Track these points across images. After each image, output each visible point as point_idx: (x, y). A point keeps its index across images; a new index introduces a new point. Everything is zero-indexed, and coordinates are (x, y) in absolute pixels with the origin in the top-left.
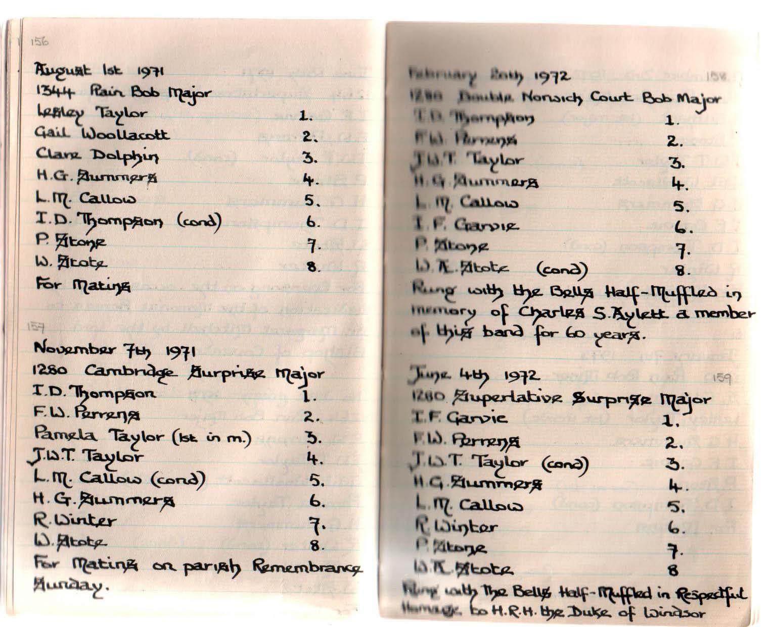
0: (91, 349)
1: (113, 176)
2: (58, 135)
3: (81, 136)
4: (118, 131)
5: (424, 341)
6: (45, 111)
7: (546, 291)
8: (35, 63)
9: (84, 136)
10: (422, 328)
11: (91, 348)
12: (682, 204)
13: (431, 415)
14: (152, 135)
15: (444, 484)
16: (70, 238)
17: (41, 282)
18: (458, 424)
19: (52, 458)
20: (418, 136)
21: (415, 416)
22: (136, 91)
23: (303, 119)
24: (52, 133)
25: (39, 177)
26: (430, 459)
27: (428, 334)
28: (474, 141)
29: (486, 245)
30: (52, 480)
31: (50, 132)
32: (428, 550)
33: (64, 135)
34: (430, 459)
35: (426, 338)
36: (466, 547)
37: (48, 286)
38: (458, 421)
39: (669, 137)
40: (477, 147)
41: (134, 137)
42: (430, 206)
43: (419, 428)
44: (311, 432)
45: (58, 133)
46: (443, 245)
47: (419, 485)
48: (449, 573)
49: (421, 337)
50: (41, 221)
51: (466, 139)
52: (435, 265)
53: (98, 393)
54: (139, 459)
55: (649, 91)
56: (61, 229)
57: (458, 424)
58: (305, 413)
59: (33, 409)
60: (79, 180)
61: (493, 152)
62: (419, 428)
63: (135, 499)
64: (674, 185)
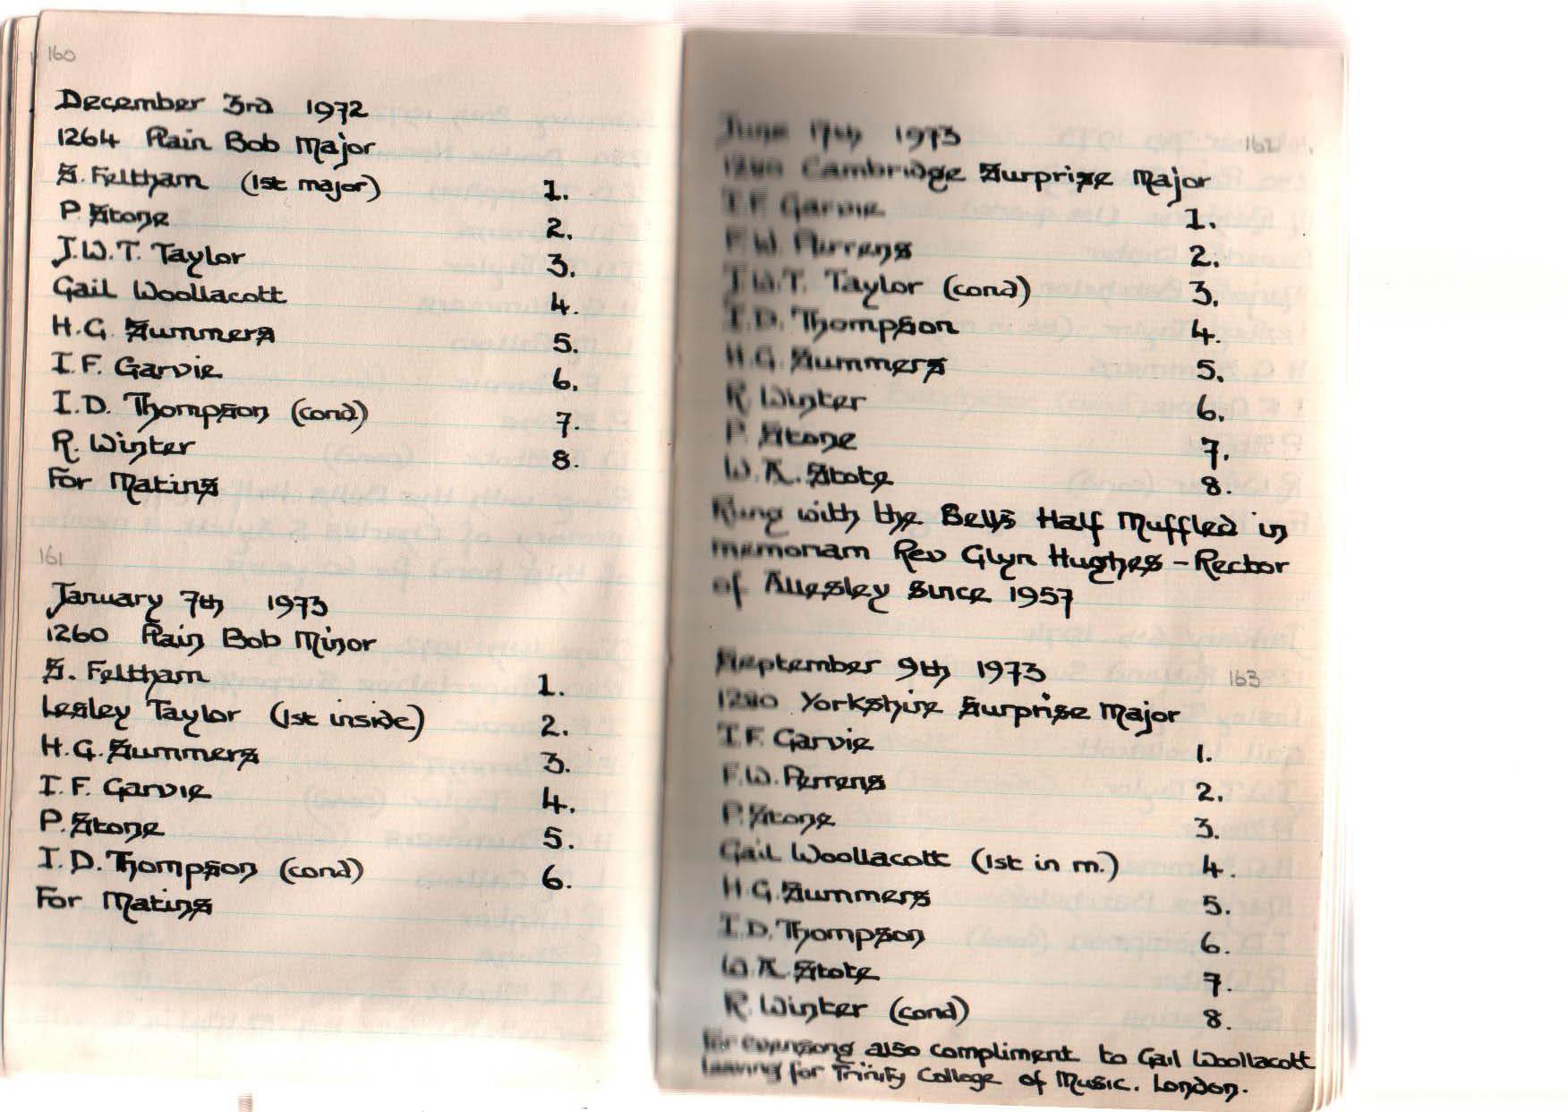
0: (159, 103)
1: (176, 751)
2: (95, 293)
3: (133, 296)
4: (193, 286)
5: (739, 603)
6: (57, 708)
7: (954, 554)
8: (60, 237)
9: (137, 297)
10: (735, 578)
11: (160, 100)
12: (1217, 901)
13: (750, 736)
14: (253, 295)
15: (774, 895)
16: (96, 820)
17: (57, 479)
18: (793, 750)
19: (93, 256)
20: (731, 238)
21: (724, 734)
22: (234, 140)
23: (545, 692)
24: (83, 292)
25: (56, 332)
26: (748, 773)
27: (746, 591)
28: (832, 248)
29: (852, 436)
30: (88, 244)
31: (80, 287)
32: (742, 822)
33: (106, 293)
34: (748, 773)
35: (743, 598)
36: (823, 436)
37: (57, 902)
38: (793, 745)
39: (550, 220)
40: (838, 260)
41: (220, 297)
42: (740, 744)
43: (730, 755)
44: (556, 754)
45: (94, 289)
46: (771, 434)
47: (733, 893)
48: (783, 977)
49: (731, 597)
50: (47, 792)
51: (817, 247)
52: (759, 469)
53: (123, 826)
54: (239, 261)
55: (1122, 1053)
56: (100, 425)
57: (793, 750)
58: (1192, 249)
59: (48, 473)
60: (111, 756)
61: (868, 270)
62: (730, 755)
63: (233, 337)
64: (1195, 334)
